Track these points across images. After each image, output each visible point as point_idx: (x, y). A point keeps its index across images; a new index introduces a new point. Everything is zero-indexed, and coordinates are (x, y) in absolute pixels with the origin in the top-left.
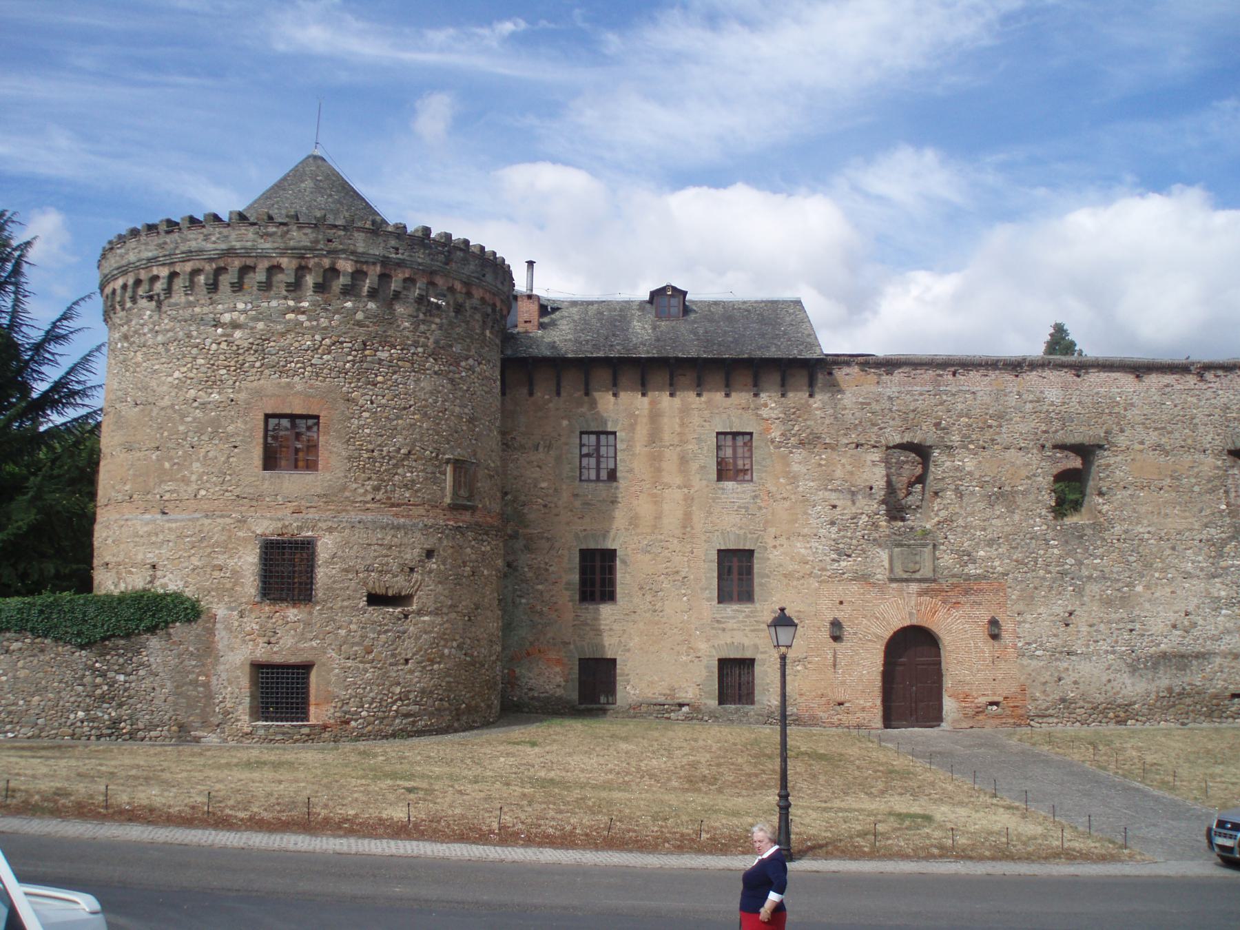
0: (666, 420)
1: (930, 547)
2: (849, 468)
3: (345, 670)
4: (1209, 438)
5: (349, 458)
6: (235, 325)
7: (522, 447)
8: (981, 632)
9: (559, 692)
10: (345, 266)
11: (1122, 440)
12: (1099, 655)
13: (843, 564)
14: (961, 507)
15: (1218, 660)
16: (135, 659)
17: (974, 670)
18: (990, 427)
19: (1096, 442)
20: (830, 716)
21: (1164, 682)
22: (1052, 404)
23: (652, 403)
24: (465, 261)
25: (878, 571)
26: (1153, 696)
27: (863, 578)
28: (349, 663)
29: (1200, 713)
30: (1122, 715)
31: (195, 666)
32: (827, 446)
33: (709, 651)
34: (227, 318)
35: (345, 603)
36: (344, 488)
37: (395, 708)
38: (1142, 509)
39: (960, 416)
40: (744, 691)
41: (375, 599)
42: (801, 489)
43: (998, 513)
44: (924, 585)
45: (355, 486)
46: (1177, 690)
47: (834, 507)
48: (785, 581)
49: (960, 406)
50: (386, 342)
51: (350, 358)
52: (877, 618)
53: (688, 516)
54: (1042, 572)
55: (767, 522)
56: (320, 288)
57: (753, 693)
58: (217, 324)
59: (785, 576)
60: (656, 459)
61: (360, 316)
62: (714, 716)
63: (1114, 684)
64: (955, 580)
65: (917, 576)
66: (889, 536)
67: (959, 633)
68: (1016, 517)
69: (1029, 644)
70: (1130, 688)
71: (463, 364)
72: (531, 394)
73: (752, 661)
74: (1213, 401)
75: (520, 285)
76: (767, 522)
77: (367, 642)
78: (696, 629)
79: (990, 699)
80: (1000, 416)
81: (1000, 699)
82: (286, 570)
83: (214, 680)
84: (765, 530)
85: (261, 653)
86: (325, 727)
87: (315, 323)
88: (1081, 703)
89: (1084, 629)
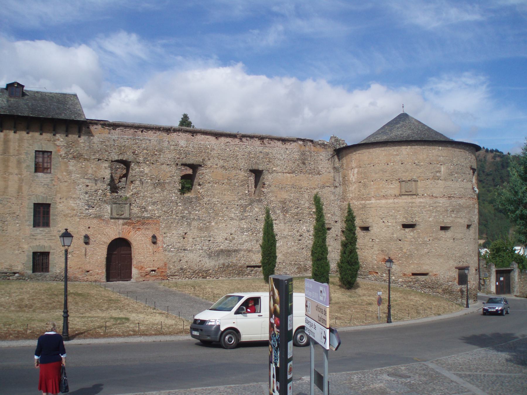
1: (129, 204)
2: (94, 169)
4: (243, 164)
8: (149, 241)
11: (209, 163)
12: (196, 250)
13: (90, 211)
14: (142, 188)
15: (242, 253)
18: (156, 155)
19: (199, 163)
21: (222, 261)
22: (182, 147)
23: (6, 135)
25: (106, 214)
26: (217, 267)
27: (99, 217)
29: (234, 273)
30: (205, 274)
32: (85, 159)
33: (28, 248)
38: (216, 192)
42: (73, 178)
43: (157, 191)
44: (126, 221)
46: (226, 264)
47: (87, 186)
48: (64, 218)
49: (144, 145)
52: (105, 235)
53: (20, 188)
54: (174, 216)
59: (64, 215)
62: (30, 278)
64: (138, 219)
65: (123, 217)
67: (139, 240)
68: (165, 193)
69: (168, 246)
70: (208, 264)
74: (245, 150)
78: (23, 239)
79: (152, 269)
80: (160, 151)
81: (156, 269)
84: (56, 195)
88: (189, 270)
89: (191, 240)
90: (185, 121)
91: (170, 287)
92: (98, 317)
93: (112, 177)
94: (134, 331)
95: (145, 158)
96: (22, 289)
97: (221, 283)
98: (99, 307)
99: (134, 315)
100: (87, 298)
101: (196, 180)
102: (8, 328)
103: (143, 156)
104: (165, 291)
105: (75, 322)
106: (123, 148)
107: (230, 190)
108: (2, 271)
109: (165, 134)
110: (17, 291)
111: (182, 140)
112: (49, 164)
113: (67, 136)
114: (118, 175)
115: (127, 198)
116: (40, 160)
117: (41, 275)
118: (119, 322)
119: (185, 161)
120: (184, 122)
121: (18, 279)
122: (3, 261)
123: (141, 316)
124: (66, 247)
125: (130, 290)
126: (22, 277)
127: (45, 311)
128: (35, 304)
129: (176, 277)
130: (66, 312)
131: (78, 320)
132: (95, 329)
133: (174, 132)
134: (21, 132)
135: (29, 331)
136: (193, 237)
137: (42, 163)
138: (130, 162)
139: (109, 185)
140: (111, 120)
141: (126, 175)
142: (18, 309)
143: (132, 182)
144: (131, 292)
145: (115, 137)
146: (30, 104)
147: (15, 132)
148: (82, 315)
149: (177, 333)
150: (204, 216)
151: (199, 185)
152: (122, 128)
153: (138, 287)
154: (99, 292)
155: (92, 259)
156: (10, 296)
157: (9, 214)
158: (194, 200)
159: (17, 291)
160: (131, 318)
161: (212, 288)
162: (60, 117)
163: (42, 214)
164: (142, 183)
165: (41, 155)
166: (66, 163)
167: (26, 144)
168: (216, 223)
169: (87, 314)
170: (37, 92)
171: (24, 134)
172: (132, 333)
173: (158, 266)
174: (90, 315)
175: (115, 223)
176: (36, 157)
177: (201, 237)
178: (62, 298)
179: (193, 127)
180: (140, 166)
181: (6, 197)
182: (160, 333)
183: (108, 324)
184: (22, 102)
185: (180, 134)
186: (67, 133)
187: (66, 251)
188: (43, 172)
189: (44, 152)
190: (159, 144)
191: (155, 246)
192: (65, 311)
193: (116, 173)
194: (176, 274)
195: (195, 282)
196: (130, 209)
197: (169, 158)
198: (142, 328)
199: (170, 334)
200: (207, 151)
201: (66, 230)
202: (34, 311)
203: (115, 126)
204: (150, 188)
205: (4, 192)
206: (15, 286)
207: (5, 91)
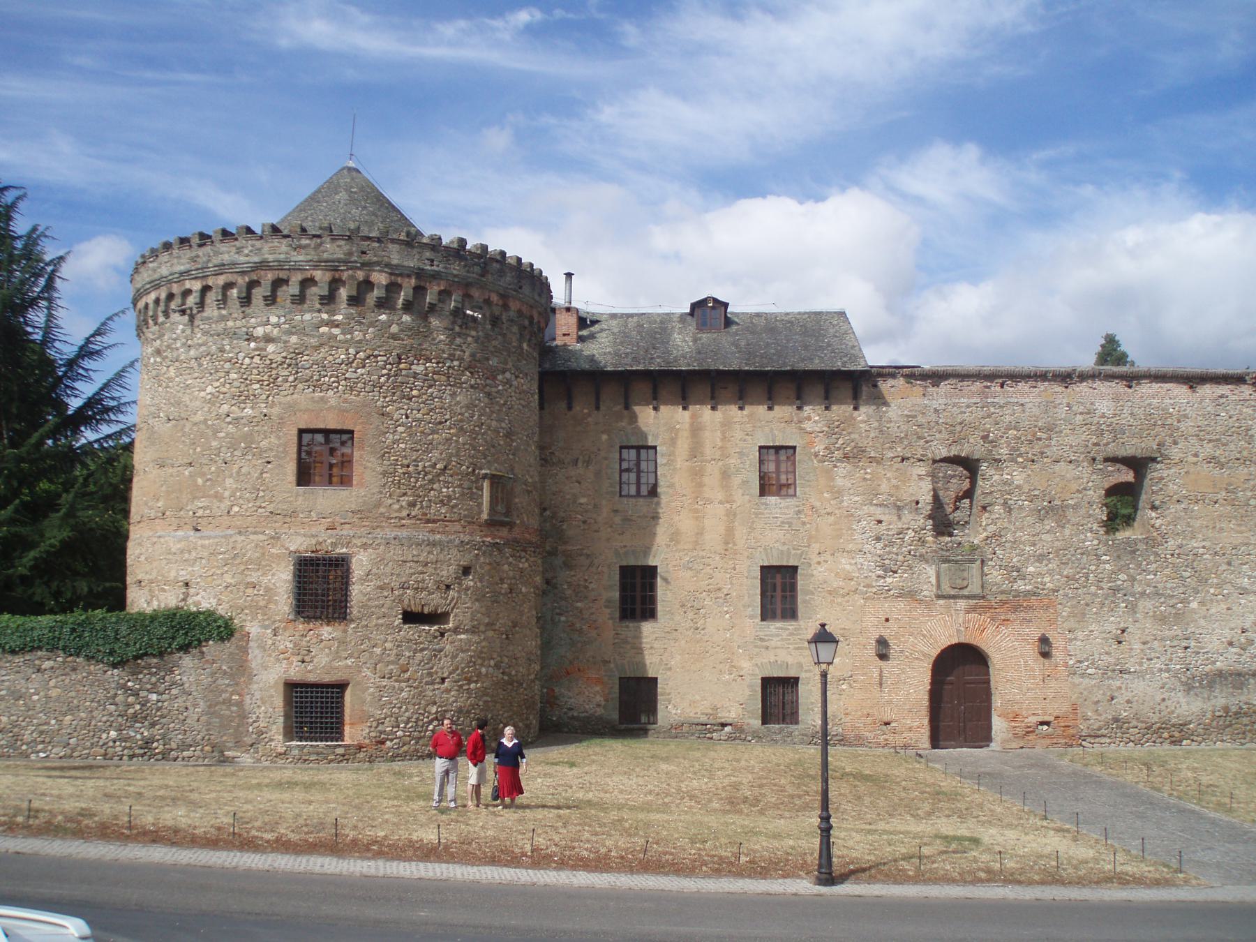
0: (707, 434)
1: (979, 562)
2: (894, 482)
3: (380, 689)
5: (384, 474)
6: (268, 339)
7: (561, 462)
8: (1032, 650)
9: (600, 711)
10: (380, 278)
11: (1175, 453)
12: (1153, 673)
13: (889, 580)
14: (1010, 522)
16: (167, 678)
17: (1024, 689)
18: (1040, 439)
19: (1148, 454)
20: (876, 736)
22: (1103, 416)
23: (693, 417)
24: (501, 273)
26: (1209, 715)
27: (910, 595)
28: (385, 682)
30: (1177, 734)
31: (228, 685)
32: (872, 460)
34: (259, 331)
35: (380, 621)
36: (379, 504)
37: (431, 727)
39: (1009, 428)
40: (788, 711)
41: (411, 617)
42: (845, 504)
43: (1048, 527)
45: (390, 501)
46: (1234, 709)
47: (880, 522)
48: (830, 598)
49: (1008, 419)
50: (421, 356)
51: (384, 372)
52: (924, 636)
53: (730, 531)
54: (1093, 589)
55: (810, 537)
56: (355, 301)
57: (797, 712)
58: (250, 338)
59: (830, 592)
60: (697, 474)
61: (394, 329)
62: (758, 737)
63: (1168, 703)
64: (1004, 597)
65: (965, 592)
66: (935, 552)
67: (1008, 650)
68: (1067, 532)
69: (1081, 662)
70: (1185, 707)
71: (500, 377)
72: (570, 408)
73: (797, 680)
75: (559, 296)
76: (810, 537)
77: (403, 661)
78: (739, 647)
79: (1041, 719)
80: (1050, 429)
82: (320, 588)
83: (247, 699)
84: (809, 546)
85: (295, 672)
86: (360, 748)
87: (349, 336)
88: (1134, 723)
89: (1137, 646)
90: (1111, 352)
91: (1086, 765)
92: (906, 833)
93: (936, 498)
94: (989, 871)
95: (1014, 450)
96: (738, 761)
97: (1221, 756)
98: (910, 808)
99: (993, 831)
100: (884, 788)
101: (1143, 497)
102: (699, 849)
103: (1009, 444)
104: (1075, 773)
105: (850, 843)
106: (958, 428)
107: (1235, 517)
108: (696, 721)
109: (1058, 388)
110: (726, 765)
111: (1103, 399)
112: (791, 476)
113: (827, 408)
114: (953, 494)
115: (974, 548)
116: (771, 467)
117: (781, 730)
118: (954, 846)
119: (1112, 450)
120: (1109, 354)
121: (730, 738)
122: (698, 697)
123: (1011, 834)
124: (824, 666)
125: (987, 770)
126: (739, 734)
127: (787, 814)
128: (764, 795)
129: (1103, 740)
130: (826, 818)
131: (857, 837)
132: (895, 861)
133: (1081, 382)
134: (727, 407)
135: (743, 859)
136: (1144, 638)
137: (776, 472)
138: (978, 460)
139: (930, 517)
140: (928, 364)
141: (969, 494)
142: (728, 807)
143: (984, 508)
144: (989, 774)
145: (938, 403)
146: (743, 343)
147: (713, 408)
148: (868, 827)
149: (1097, 883)
150: (1169, 585)
151: (1154, 508)
152: (954, 381)
153: (1006, 763)
154: (912, 774)
155: (897, 695)
156: (711, 778)
157: (709, 591)
158: (1142, 546)
159: (726, 765)
160: (986, 840)
161: (1194, 770)
162: (810, 367)
163: (779, 589)
164: (1009, 510)
165: (772, 457)
166: (828, 471)
167: (738, 434)
168: (1202, 603)
169: (882, 826)
170: (758, 315)
171: (733, 410)
172: (982, 875)
173: (1057, 713)
174: (888, 827)
175: (948, 607)
176: (761, 462)
177: (1163, 639)
178: (817, 786)
179: (1133, 364)
180: (1002, 469)
181: (701, 553)
182: (1053, 878)
183: (926, 851)
184: (725, 339)
185: (1097, 384)
186: (828, 400)
187: (824, 675)
188: (778, 494)
189: (778, 449)
190: (1046, 412)
191: (1046, 662)
192: (825, 814)
193: (947, 489)
194: (1103, 731)
195: (1151, 753)
196: (983, 574)
197: (1071, 446)
198: (1010, 864)
199: (1080, 882)
200: (1169, 421)
201: (823, 625)
202: (762, 812)
203: (936, 377)
204: (1030, 520)
205: (696, 543)
206: (722, 754)
207: (689, 318)
